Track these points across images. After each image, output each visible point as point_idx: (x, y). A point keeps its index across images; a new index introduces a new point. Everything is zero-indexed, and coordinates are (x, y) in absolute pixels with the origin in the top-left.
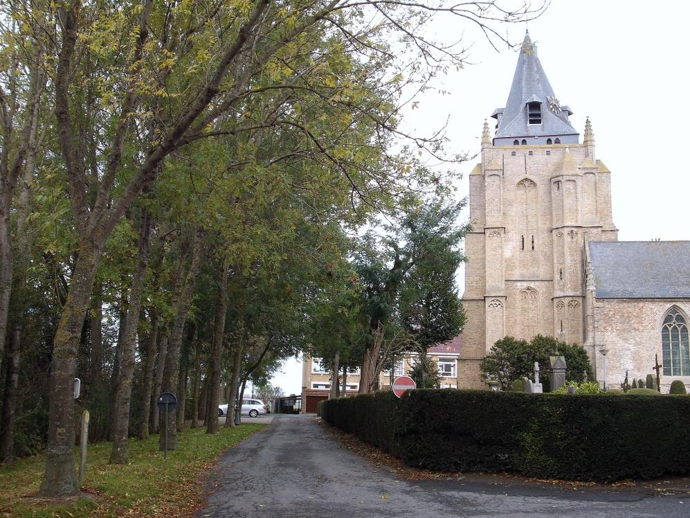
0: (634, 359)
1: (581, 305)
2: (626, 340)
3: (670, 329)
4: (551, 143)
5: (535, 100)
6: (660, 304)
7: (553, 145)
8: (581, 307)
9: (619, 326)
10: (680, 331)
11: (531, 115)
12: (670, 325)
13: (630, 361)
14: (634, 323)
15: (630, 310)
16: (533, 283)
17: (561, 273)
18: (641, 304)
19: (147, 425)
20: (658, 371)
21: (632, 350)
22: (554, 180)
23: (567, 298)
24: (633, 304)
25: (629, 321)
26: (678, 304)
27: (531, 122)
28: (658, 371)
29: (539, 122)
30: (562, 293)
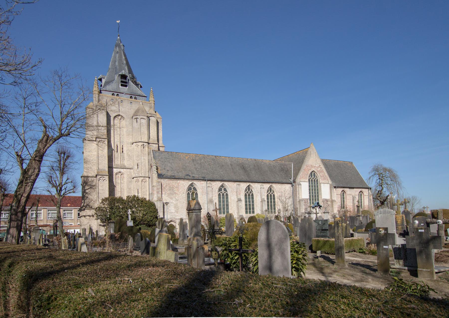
0: (175, 207)
1: (148, 181)
2: (171, 198)
3: (191, 194)
4: (132, 98)
5: (124, 74)
6: (187, 182)
7: (115, 96)
8: (148, 183)
9: (169, 192)
10: (251, 195)
11: (122, 82)
12: (221, 192)
13: (173, 208)
14: (175, 191)
15: (173, 184)
16: (123, 169)
17: (138, 165)
18: (179, 181)
19: (91, 291)
20: (216, 212)
21: (174, 203)
22: (134, 117)
23: (141, 178)
24: (175, 181)
25: (173, 189)
26: (194, 182)
27: (122, 85)
28: (216, 212)
29: (126, 86)
30: (138, 175)
